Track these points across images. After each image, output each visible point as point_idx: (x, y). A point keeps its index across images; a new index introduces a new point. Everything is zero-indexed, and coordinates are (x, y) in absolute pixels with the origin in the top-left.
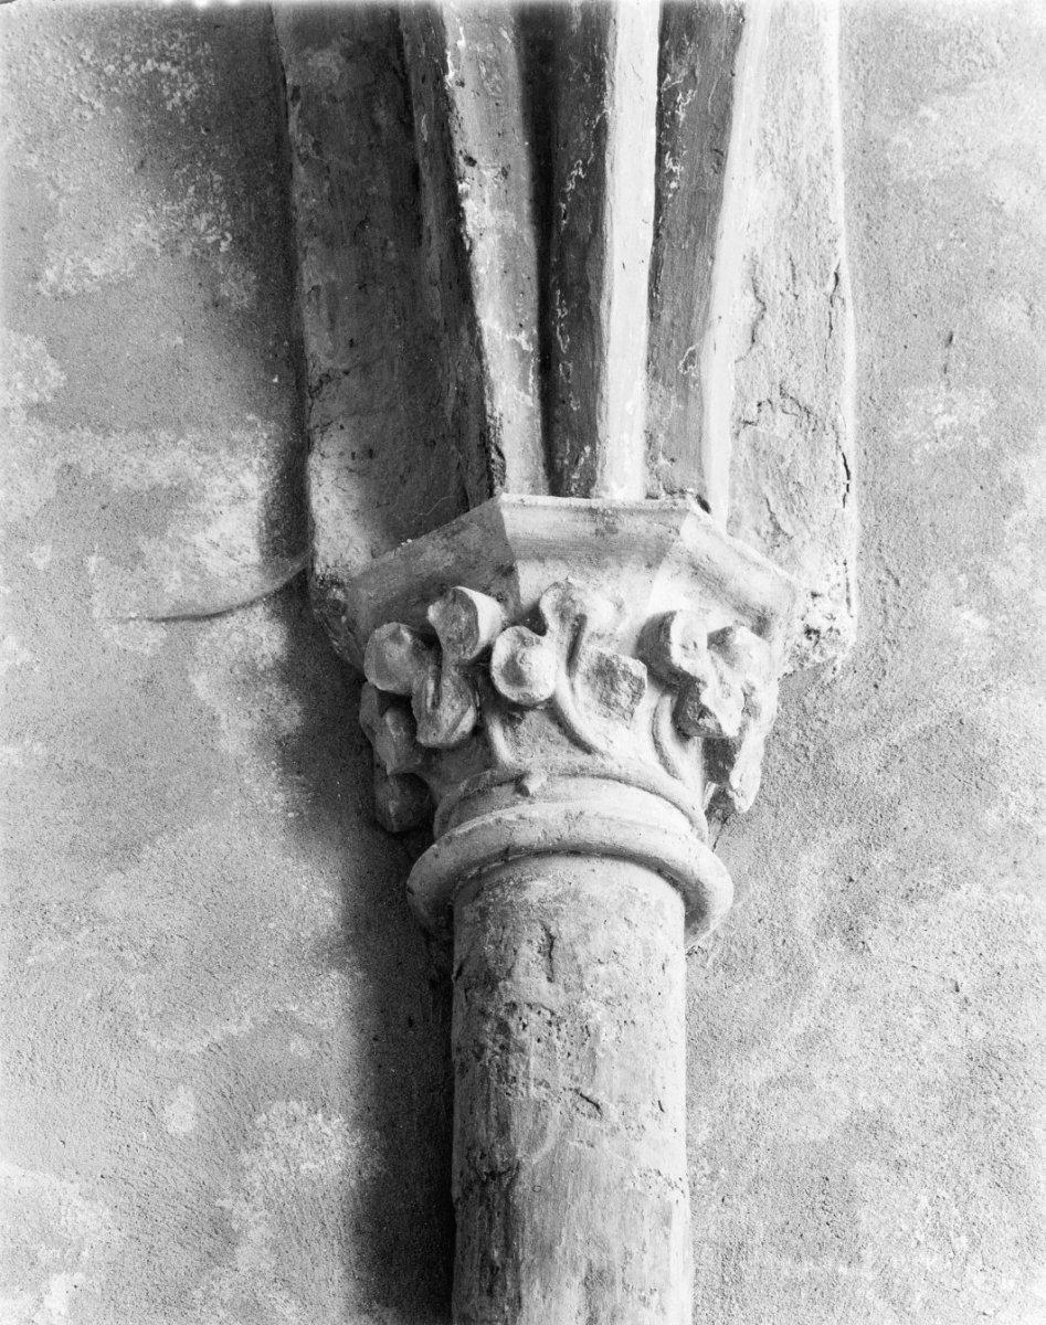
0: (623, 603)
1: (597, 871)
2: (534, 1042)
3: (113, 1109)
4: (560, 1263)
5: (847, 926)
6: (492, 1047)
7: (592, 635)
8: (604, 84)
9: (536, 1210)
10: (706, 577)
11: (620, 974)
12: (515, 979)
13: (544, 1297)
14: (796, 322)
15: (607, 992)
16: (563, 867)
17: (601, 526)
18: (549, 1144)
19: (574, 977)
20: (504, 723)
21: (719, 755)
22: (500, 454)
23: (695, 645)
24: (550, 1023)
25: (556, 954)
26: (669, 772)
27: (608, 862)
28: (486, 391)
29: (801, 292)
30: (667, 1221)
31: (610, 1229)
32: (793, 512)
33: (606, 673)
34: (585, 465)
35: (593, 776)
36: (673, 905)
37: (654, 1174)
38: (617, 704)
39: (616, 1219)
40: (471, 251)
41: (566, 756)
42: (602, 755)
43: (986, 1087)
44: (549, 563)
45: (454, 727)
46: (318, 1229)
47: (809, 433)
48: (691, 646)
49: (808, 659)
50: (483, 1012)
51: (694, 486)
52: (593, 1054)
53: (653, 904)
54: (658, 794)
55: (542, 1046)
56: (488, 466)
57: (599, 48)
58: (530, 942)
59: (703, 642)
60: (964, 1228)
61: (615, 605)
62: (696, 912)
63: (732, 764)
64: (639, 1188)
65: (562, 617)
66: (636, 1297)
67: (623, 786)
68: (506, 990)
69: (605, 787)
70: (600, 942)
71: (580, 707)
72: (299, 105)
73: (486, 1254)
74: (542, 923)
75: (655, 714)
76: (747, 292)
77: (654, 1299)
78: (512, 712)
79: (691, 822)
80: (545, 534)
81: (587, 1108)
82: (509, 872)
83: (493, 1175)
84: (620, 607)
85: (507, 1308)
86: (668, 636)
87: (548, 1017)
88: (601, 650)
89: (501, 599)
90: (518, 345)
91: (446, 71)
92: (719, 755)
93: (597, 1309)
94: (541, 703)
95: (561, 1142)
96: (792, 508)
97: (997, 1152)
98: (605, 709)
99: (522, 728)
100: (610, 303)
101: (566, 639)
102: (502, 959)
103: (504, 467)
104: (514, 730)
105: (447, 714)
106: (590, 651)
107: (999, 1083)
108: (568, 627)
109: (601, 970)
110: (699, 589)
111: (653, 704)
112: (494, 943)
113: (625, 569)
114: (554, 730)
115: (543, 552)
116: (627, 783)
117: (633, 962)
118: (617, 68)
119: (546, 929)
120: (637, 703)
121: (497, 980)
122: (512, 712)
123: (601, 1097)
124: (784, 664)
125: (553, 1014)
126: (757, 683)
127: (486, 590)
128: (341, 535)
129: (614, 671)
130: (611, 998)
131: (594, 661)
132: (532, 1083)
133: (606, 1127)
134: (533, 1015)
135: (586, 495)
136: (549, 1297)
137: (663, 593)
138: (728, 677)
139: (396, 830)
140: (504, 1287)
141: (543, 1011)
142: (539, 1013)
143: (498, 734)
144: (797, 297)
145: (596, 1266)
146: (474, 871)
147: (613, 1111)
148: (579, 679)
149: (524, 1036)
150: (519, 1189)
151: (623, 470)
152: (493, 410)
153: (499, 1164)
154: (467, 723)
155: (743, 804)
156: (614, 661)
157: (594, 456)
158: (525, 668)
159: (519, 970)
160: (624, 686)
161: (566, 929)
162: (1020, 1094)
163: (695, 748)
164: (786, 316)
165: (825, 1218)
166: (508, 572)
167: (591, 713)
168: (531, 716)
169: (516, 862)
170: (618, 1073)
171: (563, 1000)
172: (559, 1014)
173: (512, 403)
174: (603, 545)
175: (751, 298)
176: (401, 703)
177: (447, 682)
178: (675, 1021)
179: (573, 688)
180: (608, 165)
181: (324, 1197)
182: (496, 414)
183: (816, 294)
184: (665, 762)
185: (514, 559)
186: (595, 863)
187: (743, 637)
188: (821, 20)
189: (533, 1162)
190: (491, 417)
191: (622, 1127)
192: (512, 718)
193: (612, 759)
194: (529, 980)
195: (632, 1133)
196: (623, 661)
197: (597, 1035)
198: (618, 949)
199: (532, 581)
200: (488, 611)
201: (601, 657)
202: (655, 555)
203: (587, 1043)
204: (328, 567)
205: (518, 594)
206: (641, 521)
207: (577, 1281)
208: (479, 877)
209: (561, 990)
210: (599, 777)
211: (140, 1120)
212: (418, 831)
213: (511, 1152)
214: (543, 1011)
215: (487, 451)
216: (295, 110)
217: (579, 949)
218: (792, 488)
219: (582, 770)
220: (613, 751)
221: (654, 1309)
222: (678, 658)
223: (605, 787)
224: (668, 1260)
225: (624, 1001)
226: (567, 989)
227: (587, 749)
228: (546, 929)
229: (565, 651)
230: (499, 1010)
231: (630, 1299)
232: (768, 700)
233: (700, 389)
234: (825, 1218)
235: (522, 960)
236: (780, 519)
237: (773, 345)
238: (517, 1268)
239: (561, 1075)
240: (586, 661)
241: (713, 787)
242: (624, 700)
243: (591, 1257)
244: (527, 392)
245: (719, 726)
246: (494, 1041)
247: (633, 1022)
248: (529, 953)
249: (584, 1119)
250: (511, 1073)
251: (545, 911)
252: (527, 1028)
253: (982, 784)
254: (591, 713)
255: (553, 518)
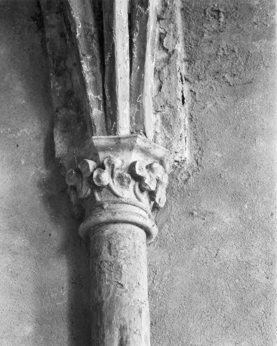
0: (123, 160)
1: (121, 227)
2: (107, 270)
3: (11, 293)
4: (113, 325)
5: (189, 233)
6: (97, 272)
7: (117, 168)
8: (113, 34)
9: (108, 312)
10: (145, 152)
11: (127, 252)
12: (102, 255)
13: (110, 334)
14: (170, 85)
15: (124, 256)
16: (112, 226)
17: (117, 142)
18: (111, 295)
19: (116, 254)
20: (98, 192)
21: (152, 195)
22: (94, 126)
23: (142, 169)
24: (110, 265)
25: (112, 248)
26: (139, 200)
27: (124, 224)
28: (90, 111)
29: (171, 77)
30: (140, 312)
31: (126, 315)
32: (170, 132)
33: (121, 178)
34: (114, 127)
35: (119, 203)
36: (142, 233)
37: (137, 301)
38: (125, 185)
39: (127, 313)
40: (85, 77)
41: (112, 198)
42: (121, 198)
43: (224, 271)
44: (106, 152)
45: (86, 194)
46: (61, 319)
47: (173, 112)
48: (141, 169)
49: (177, 168)
50: (95, 264)
51: (142, 129)
52: (121, 272)
53: (136, 233)
54: (136, 206)
55: (109, 271)
56: (92, 129)
57: (112, 26)
58: (105, 245)
59: (144, 168)
60: (219, 307)
61: (121, 161)
62: (148, 234)
63: (155, 196)
64: (133, 305)
65: (109, 165)
66: (133, 332)
67: (127, 205)
68: (100, 258)
69: (122, 205)
70: (122, 244)
71: (115, 186)
72: (49, 43)
73: (97, 324)
74: (108, 240)
75: (134, 186)
76: (158, 79)
77: (138, 332)
78: (99, 189)
79: (146, 212)
80: (104, 145)
81: (119, 286)
82: (100, 228)
83: (98, 304)
84: (123, 161)
85: (101, 337)
86: (135, 167)
87: (110, 264)
88: (119, 172)
89: (96, 161)
90: (97, 99)
91: (77, 34)
92: (152, 195)
93: (123, 336)
94: (106, 186)
95: (114, 295)
96: (170, 132)
97: (227, 287)
98: (122, 186)
99: (102, 192)
100: (118, 87)
101: (110, 170)
102: (99, 250)
103: (95, 129)
104: (100, 193)
105: (84, 191)
106: (117, 172)
107: (227, 270)
108: (111, 167)
109: (122, 251)
110: (144, 155)
111: (134, 184)
112: (97, 246)
113: (125, 152)
114: (110, 192)
115: (104, 149)
116: (128, 204)
117: (131, 248)
118: (116, 30)
119: (109, 242)
120: (129, 184)
121: (98, 255)
122: (99, 189)
123: (123, 283)
124: (171, 169)
125: (111, 263)
126: (160, 177)
127: (92, 159)
128: (60, 147)
129: (123, 177)
130: (125, 258)
131: (118, 175)
132: (106, 281)
133: (124, 290)
134: (106, 264)
135: (115, 135)
136: (111, 333)
137: (135, 157)
138: (152, 176)
139: (77, 218)
140: (101, 332)
141: (109, 262)
142: (108, 263)
143: (97, 195)
144: (170, 79)
145: (122, 325)
146: (93, 229)
147: (126, 286)
148: (115, 180)
149: (105, 269)
150: (104, 307)
151: (124, 127)
152: (92, 115)
153: (99, 301)
154: (89, 192)
155: (162, 205)
156: (122, 175)
157: (116, 125)
158: (101, 178)
159: (103, 253)
160: (126, 180)
161: (114, 242)
162: (232, 272)
163: (146, 193)
164: (168, 84)
165: (185, 307)
166: (97, 155)
167: (118, 188)
168: (104, 189)
169: (102, 226)
170: (127, 276)
171: (113, 259)
172: (112, 263)
173: (96, 112)
174: (118, 146)
175: (159, 81)
176: (74, 188)
177: (84, 182)
178: (143, 262)
179: (113, 182)
180: (115, 54)
181: (63, 311)
182: (93, 116)
183: (175, 78)
184: (137, 198)
185: (98, 151)
186: (120, 225)
187: (156, 165)
188: (175, 10)
189: (107, 300)
190: (92, 117)
191: (128, 290)
192: (100, 190)
193: (123, 198)
194: (105, 255)
195: (131, 291)
196: (125, 174)
197: (122, 268)
198: (126, 246)
199: (102, 155)
200: (91, 164)
201: (119, 174)
202: (131, 148)
203: (119, 270)
204: (58, 155)
205: (99, 160)
206: (127, 140)
207: (117, 329)
208: (94, 230)
209: (113, 257)
210: (121, 203)
211: (18, 295)
212: (81, 218)
213: (102, 298)
214: (109, 262)
215: (91, 125)
216: (48, 44)
217: (117, 246)
218: (169, 127)
219: (117, 202)
220: (124, 196)
221: (138, 334)
222: (138, 172)
223: (122, 205)
224: (141, 322)
225: (128, 258)
226: (114, 257)
227: (118, 196)
228: (109, 242)
229: (111, 173)
230: (99, 263)
231: (131, 332)
232: (165, 180)
233: (142, 105)
234: (185, 307)
235: (104, 250)
236: (167, 135)
237: (164, 91)
238: (103, 327)
239: (113, 279)
240: (116, 175)
241: (153, 203)
242: (126, 184)
243: (121, 323)
244: (100, 110)
245: (150, 188)
246: (98, 271)
247: (131, 264)
248: (105, 248)
249: (119, 289)
250: (101, 279)
251: (109, 238)
252: (105, 267)
253: (221, 195)
254: (118, 188)
255: (106, 141)
